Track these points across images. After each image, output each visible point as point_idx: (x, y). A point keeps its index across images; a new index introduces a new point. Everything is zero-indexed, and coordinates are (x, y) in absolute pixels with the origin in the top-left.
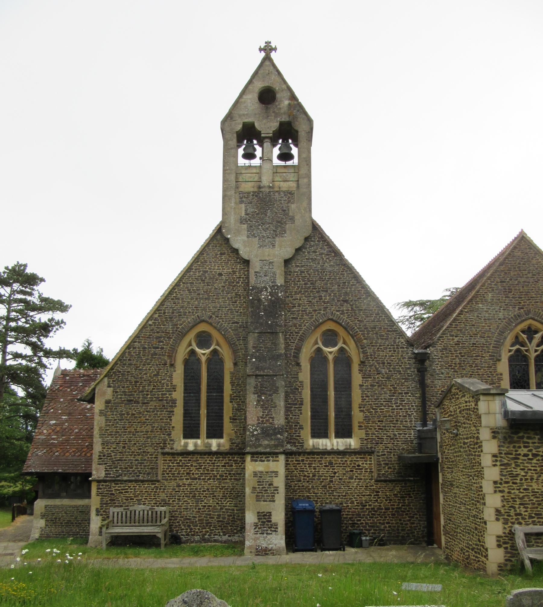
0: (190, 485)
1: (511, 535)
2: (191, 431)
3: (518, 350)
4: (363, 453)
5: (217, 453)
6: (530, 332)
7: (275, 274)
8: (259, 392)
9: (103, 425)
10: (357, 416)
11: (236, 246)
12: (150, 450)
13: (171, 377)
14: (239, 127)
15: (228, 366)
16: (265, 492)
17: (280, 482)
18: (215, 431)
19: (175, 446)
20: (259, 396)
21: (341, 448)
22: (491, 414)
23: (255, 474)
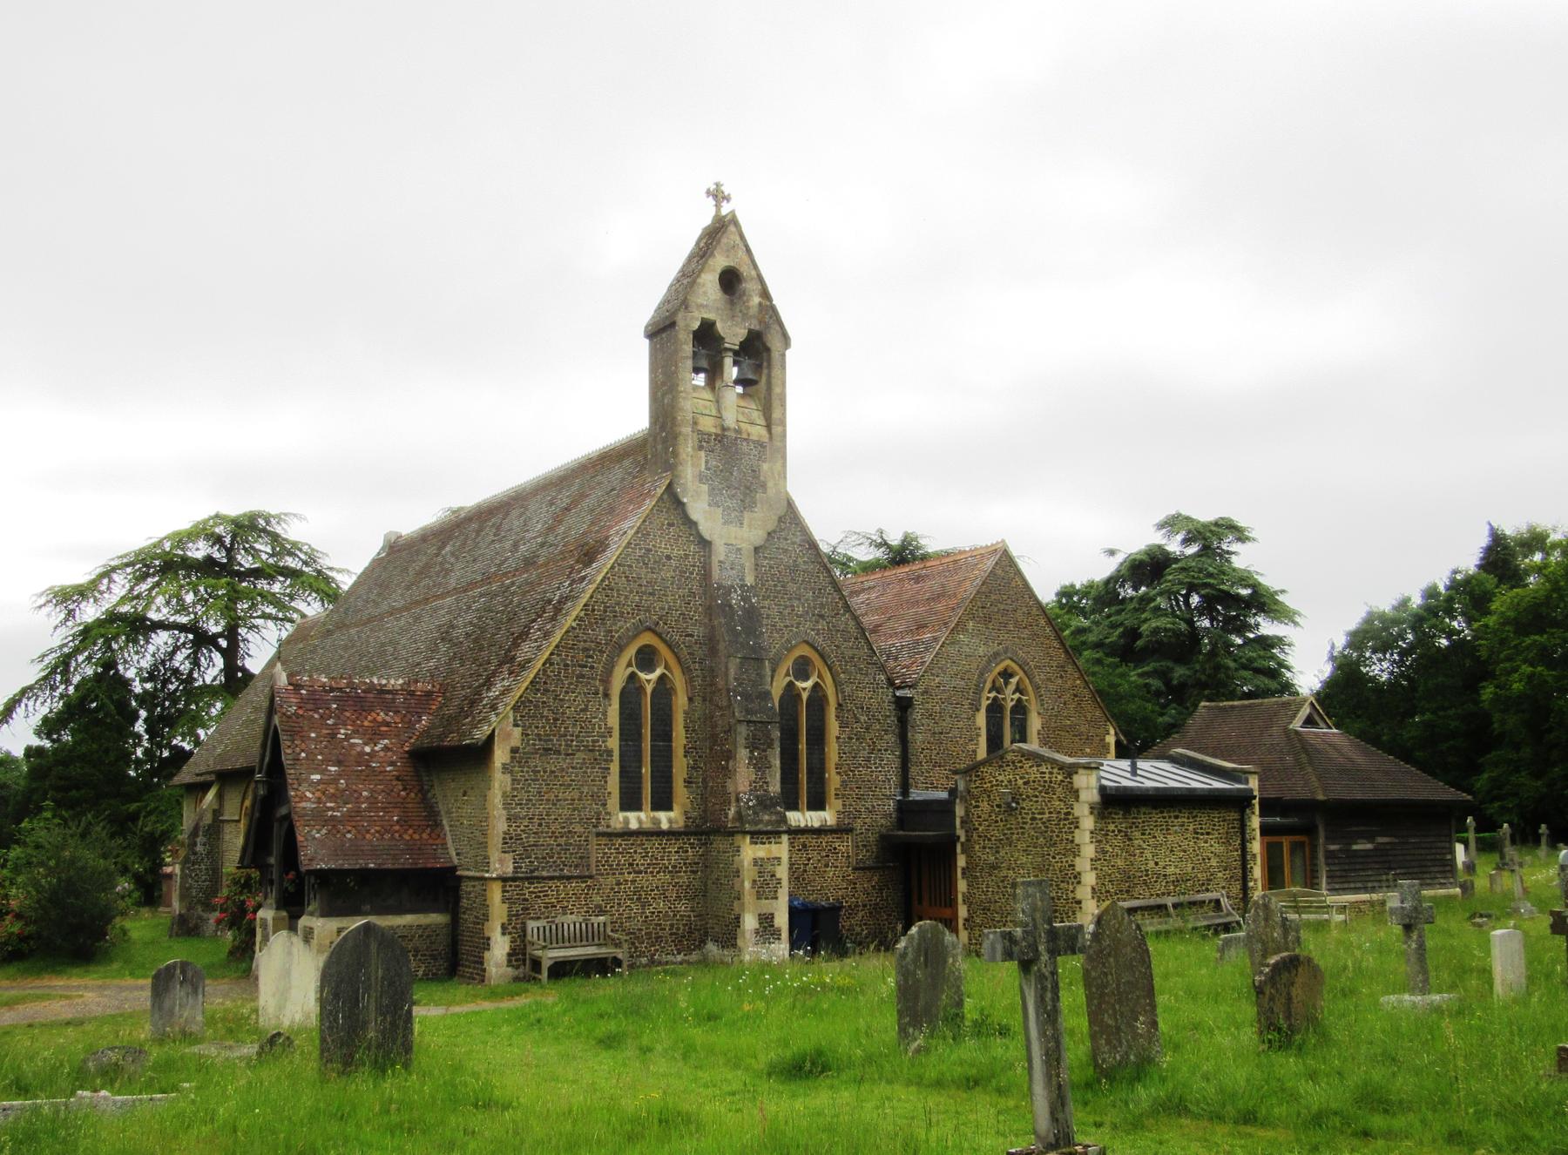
0: (633, 881)
2: (630, 801)
3: (995, 699)
4: (840, 830)
5: (670, 834)
6: (1007, 675)
8: (752, 747)
10: (834, 780)
11: (694, 516)
12: (578, 829)
13: (605, 714)
14: (696, 325)
15: (681, 701)
16: (765, 887)
17: (783, 872)
18: (663, 801)
19: (612, 823)
21: (816, 824)
22: (1088, 786)
23: (755, 861)
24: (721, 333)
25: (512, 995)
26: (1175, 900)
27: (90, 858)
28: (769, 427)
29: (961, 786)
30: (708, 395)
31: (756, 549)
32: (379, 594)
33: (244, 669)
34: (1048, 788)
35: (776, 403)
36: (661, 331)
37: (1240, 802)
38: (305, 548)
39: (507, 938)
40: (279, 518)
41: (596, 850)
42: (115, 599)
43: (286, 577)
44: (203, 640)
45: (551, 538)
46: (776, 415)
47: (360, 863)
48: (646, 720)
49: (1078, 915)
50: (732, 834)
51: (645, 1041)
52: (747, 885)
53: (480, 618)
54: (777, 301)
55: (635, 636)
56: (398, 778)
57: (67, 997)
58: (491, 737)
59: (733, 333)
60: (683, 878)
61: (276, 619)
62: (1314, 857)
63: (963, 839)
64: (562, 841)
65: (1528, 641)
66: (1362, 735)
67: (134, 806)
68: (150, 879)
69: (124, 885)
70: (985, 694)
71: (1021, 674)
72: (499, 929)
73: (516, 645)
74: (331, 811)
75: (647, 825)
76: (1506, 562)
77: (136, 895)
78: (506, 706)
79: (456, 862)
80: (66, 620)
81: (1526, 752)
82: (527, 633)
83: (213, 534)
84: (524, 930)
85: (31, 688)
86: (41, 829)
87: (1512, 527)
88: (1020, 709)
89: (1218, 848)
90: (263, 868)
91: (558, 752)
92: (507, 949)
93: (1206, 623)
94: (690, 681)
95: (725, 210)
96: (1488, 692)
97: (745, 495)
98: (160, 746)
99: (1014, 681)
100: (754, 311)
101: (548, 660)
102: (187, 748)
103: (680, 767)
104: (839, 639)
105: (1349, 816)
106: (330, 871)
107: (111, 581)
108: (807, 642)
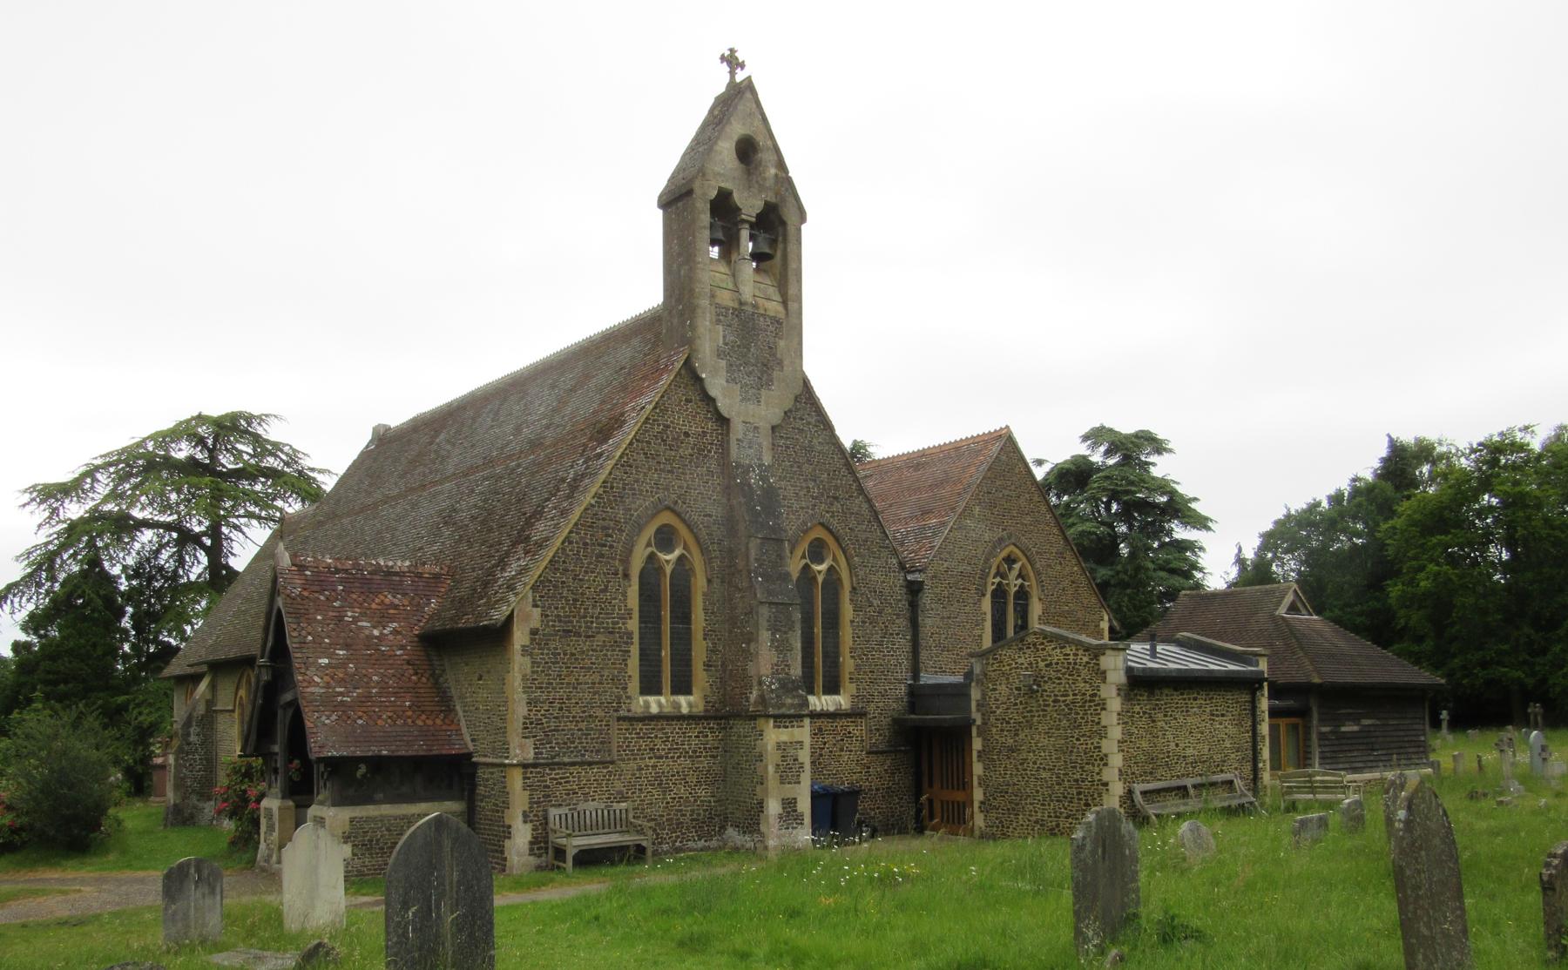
0: (654, 767)
1: (1130, 792)
2: (650, 686)
3: (1000, 584)
4: (855, 714)
5: (690, 718)
6: (1010, 560)
7: (760, 445)
8: (774, 629)
9: (529, 671)
10: (848, 664)
11: (713, 393)
12: (600, 713)
13: (624, 594)
14: (713, 194)
15: (700, 583)
16: (789, 772)
17: (805, 756)
18: (682, 686)
20: (773, 634)
21: (832, 709)
22: (1115, 666)
24: (734, 207)
25: (539, 885)
26: (1198, 780)
27: (84, 749)
28: (785, 303)
29: (977, 670)
30: (723, 268)
31: (773, 428)
32: (371, 485)
33: (227, 567)
34: (1072, 670)
35: (792, 278)
36: (675, 200)
37: (1249, 684)
38: (286, 449)
39: (529, 826)
40: (261, 419)
41: (616, 734)
42: (98, 498)
43: (267, 477)
44: (187, 539)
45: (557, 420)
46: (792, 291)
47: (373, 750)
48: (665, 601)
49: (1105, 797)
50: (754, 718)
51: (738, 942)
52: (771, 769)
53: (485, 501)
54: (793, 173)
55: (654, 516)
56: (408, 663)
57: (64, 893)
58: (510, 617)
59: (750, 205)
60: (704, 763)
61: (259, 518)
62: (1307, 738)
63: (979, 722)
64: (583, 725)
65: (1434, 540)
66: (1337, 621)
67: (121, 699)
68: (140, 769)
69: (117, 776)
70: (990, 580)
71: (1024, 560)
72: (520, 818)
73: (529, 524)
74: (339, 701)
75: (668, 710)
76: (1403, 471)
77: (126, 785)
78: (525, 588)
79: (471, 748)
80: (50, 518)
81: (1428, 645)
82: (541, 512)
83: (195, 435)
84: (546, 818)
85: (16, 585)
86: (35, 719)
87: (1407, 437)
88: (1022, 594)
89: (1232, 730)
90: (268, 756)
91: (578, 634)
92: (529, 838)
93: (1123, 529)
94: (708, 561)
95: (740, 76)
96: (1395, 590)
97: (763, 372)
98: (147, 642)
99: (1017, 566)
100: (770, 183)
101: (567, 540)
102: (174, 643)
103: (699, 651)
104: (853, 523)
105: (1343, 698)
106: (342, 758)
107: (95, 480)
108: (822, 524)
